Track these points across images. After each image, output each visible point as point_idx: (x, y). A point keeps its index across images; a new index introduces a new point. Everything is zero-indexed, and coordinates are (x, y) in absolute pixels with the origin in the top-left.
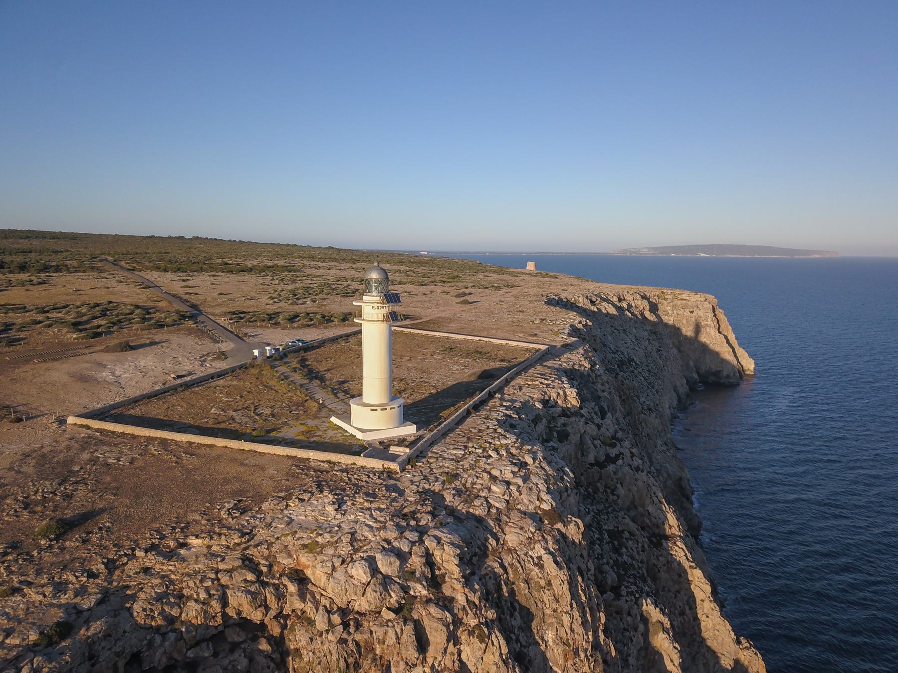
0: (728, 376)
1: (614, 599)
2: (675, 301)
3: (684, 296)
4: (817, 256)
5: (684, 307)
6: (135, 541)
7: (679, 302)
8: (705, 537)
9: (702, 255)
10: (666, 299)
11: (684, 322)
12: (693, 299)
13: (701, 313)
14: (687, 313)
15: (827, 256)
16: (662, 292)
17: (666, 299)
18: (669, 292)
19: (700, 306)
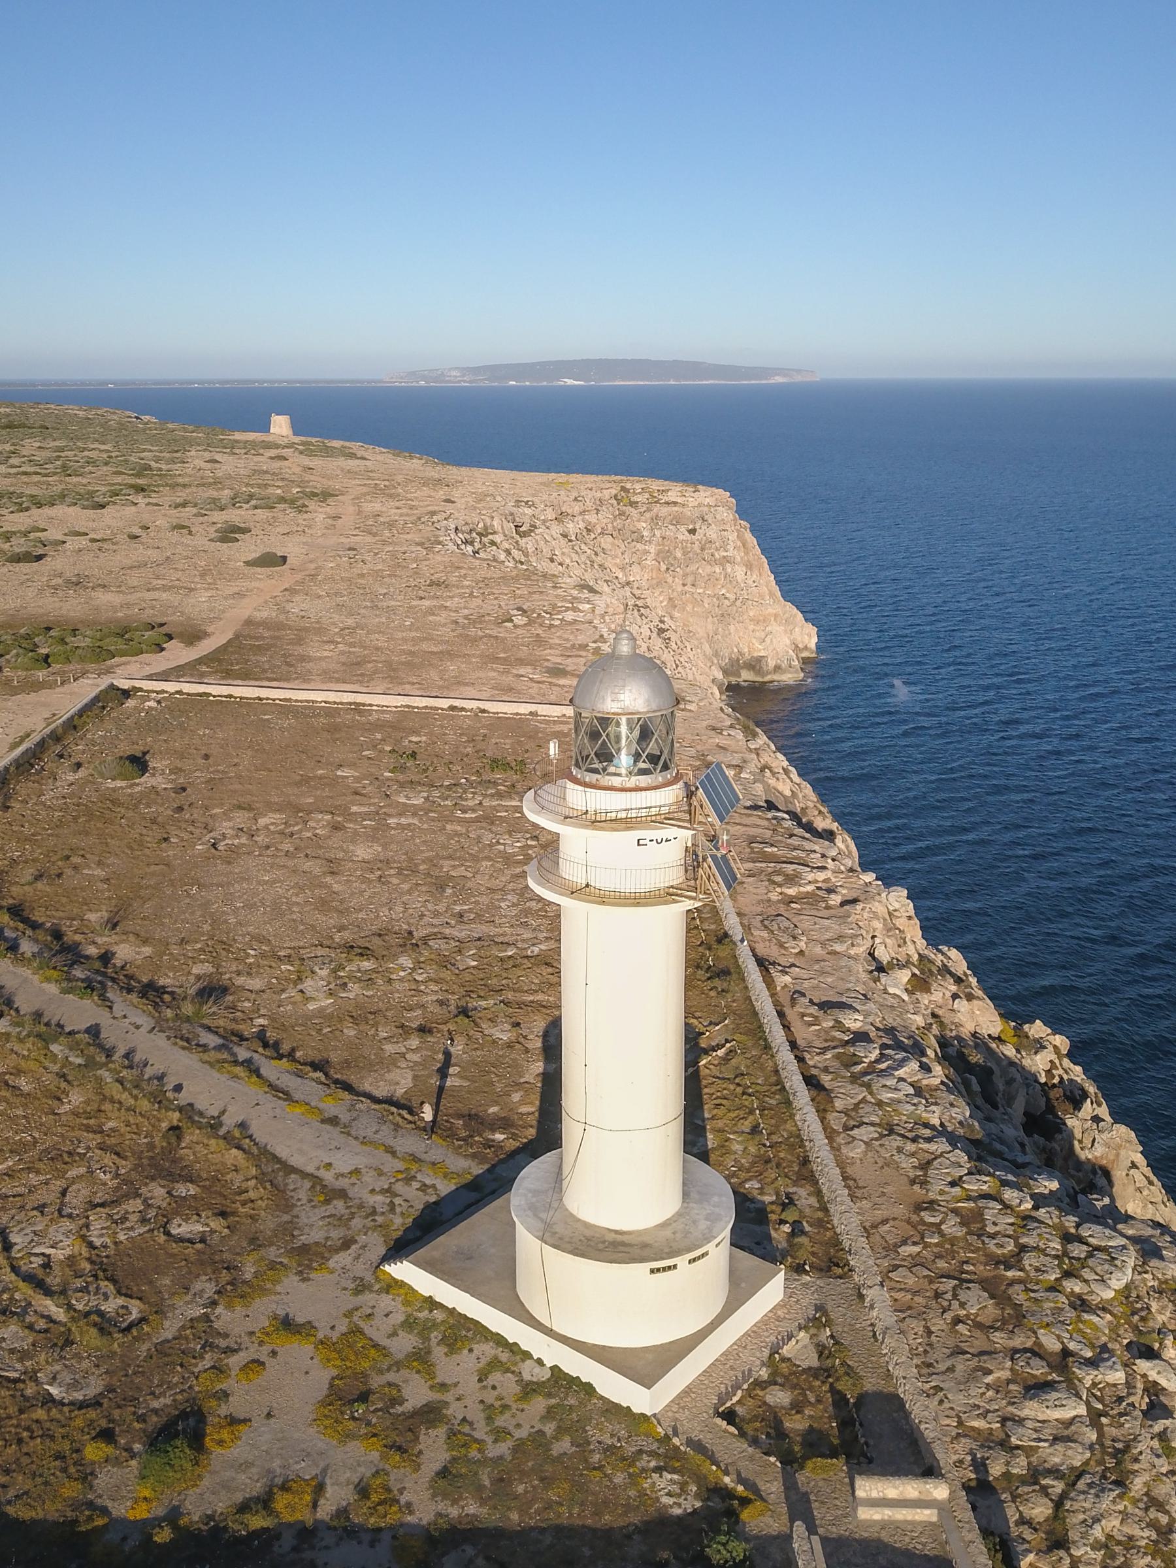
0: (777, 668)
1: (1076, 1098)
2: (656, 508)
3: (672, 496)
4: (779, 379)
5: (677, 521)
6: (388, 1190)
7: (665, 511)
8: (539, 1024)
9: (570, 382)
10: (633, 504)
11: (679, 554)
12: (692, 502)
13: (712, 533)
14: (683, 535)
15: (798, 378)
16: (623, 489)
17: (633, 504)
18: (638, 487)
19: (709, 518)
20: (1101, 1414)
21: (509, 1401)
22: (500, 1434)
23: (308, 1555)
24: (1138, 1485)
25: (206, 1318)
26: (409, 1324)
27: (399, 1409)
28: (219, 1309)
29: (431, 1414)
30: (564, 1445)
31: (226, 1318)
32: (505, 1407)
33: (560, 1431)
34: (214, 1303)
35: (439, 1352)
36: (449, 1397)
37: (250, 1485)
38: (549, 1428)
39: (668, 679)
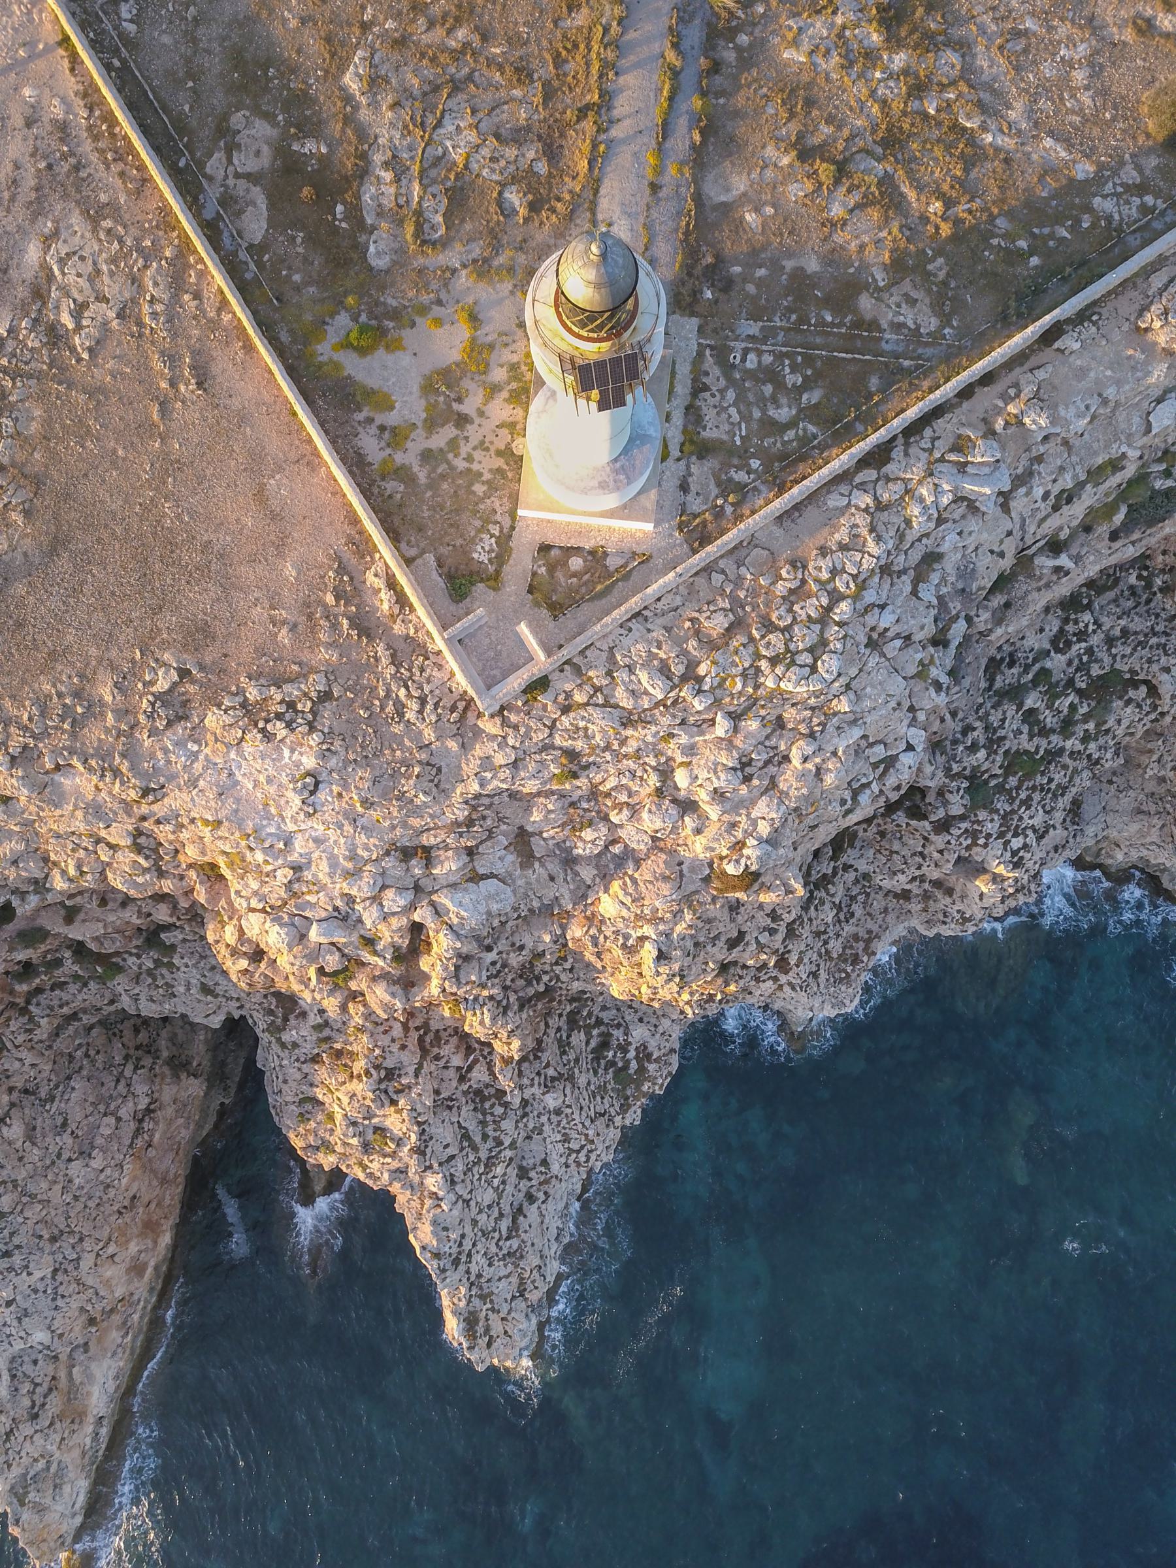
20: (665, 706)
21: (493, 449)
22: (469, 459)
23: (360, 429)
24: (629, 732)
25: (454, 271)
26: (514, 367)
27: (455, 406)
28: (464, 272)
29: (462, 420)
30: (479, 489)
31: (464, 279)
32: (487, 449)
33: (488, 482)
34: (465, 266)
35: (505, 394)
36: (477, 421)
37: (373, 383)
38: (487, 476)
39: (695, 181)
